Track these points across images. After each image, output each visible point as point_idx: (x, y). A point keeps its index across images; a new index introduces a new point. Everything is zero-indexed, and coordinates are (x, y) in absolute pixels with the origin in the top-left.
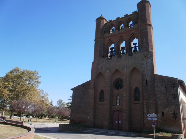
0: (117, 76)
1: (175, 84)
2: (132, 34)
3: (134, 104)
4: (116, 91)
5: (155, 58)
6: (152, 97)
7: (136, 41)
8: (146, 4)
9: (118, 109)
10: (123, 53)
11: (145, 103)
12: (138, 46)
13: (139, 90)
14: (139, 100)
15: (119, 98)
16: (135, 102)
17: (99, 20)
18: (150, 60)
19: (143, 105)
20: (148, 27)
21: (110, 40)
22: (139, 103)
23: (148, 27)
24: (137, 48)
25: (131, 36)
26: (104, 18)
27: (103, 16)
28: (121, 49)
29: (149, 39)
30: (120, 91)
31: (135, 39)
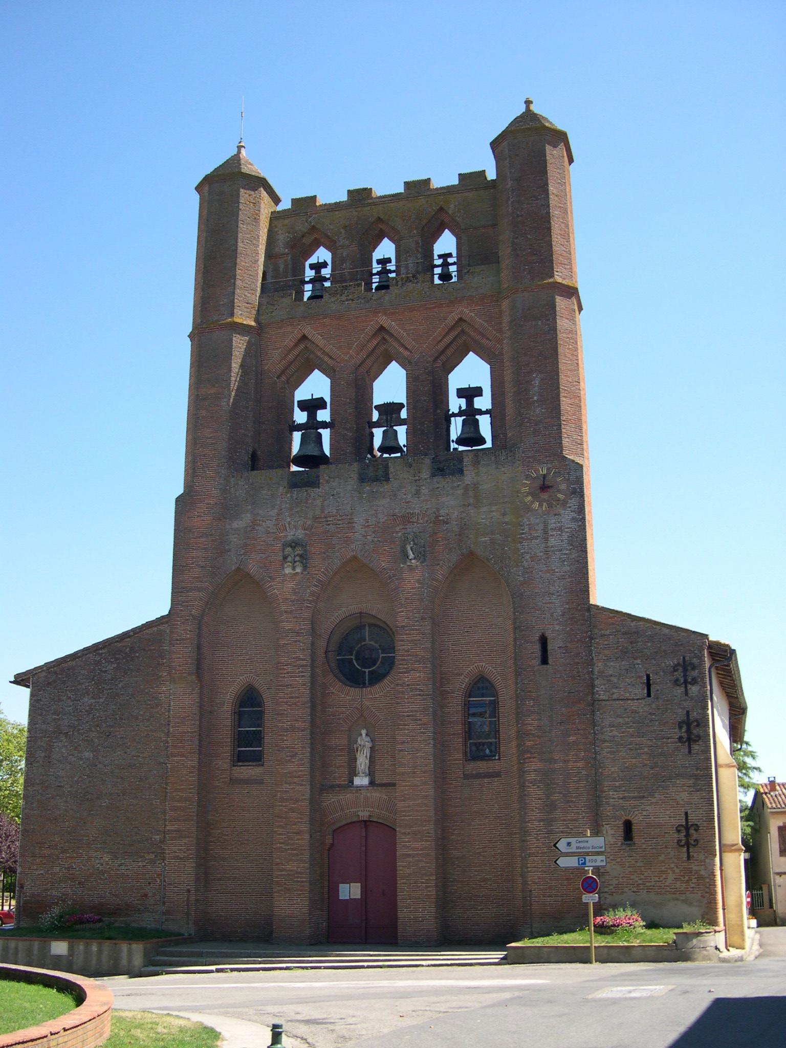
0: (352, 602)
1: (693, 669)
2: (452, 328)
3: (466, 777)
4: (345, 697)
5: (590, 512)
6: (572, 739)
7: (472, 371)
8: (553, 154)
9: (364, 815)
10: (390, 446)
11: (532, 776)
12: (487, 412)
13: (495, 695)
14: (495, 751)
15: (364, 740)
16: (472, 767)
17: (226, 189)
18: (567, 516)
19: (522, 786)
20: (561, 303)
21: (302, 346)
22: (498, 775)
23: (561, 303)
24: (485, 425)
25: (447, 340)
26: (260, 183)
27: (255, 163)
28: (375, 416)
29: (563, 379)
30: (373, 697)
31: (471, 353)
